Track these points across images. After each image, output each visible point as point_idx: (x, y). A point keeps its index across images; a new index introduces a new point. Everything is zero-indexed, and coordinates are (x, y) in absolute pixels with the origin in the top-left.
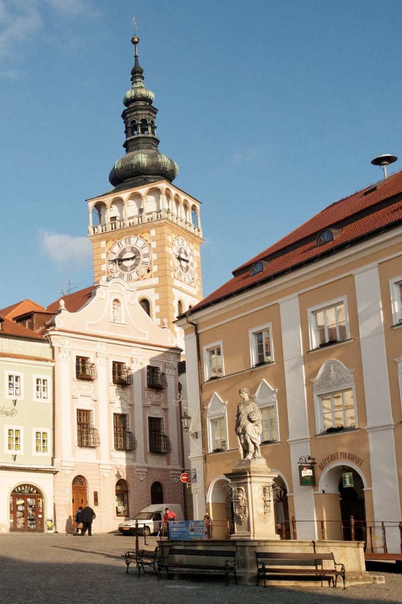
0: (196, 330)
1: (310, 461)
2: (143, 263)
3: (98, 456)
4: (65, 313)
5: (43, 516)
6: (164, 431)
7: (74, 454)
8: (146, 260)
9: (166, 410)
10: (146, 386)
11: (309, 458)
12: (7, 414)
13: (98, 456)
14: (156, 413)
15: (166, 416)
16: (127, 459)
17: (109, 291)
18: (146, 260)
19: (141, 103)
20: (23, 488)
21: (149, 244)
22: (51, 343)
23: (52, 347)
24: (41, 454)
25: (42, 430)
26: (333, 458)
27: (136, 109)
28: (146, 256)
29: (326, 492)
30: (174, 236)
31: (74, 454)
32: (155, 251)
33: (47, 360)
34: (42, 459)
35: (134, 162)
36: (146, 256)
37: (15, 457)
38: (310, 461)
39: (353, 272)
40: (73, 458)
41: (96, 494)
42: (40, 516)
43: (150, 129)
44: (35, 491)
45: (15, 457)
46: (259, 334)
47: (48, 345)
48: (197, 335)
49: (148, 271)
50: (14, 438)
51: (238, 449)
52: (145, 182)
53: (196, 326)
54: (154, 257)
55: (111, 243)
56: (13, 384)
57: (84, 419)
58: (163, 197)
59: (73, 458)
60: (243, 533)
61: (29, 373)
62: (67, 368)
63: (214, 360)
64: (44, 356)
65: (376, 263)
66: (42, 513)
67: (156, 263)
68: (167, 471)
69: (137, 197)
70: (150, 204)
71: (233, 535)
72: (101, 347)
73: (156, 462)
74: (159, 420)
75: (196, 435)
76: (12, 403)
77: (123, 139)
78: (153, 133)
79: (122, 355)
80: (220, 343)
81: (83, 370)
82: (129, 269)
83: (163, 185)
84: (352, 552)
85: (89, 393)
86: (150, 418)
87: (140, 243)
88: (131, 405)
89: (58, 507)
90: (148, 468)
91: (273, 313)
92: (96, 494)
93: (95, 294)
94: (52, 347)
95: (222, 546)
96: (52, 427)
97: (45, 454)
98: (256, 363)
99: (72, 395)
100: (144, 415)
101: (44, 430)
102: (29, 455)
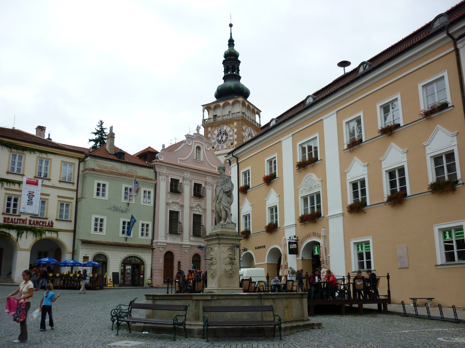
0: (238, 160)
1: (295, 239)
2: (230, 140)
5: (144, 277)
8: (231, 138)
10: (193, 195)
11: (295, 237)
12: (122, 212)
14: (175, 208)
17: (194, 141)
18: (231, 138)
20: (131, 259)
21: (233, 130)
22: (155, 169)
23: (156, 172)
24: (144, 237)
25: (146, 223)
26: (308, 236)
28: (231, 136)
29: (304, 258)
30: (246, 126)
31: (166, 238)
32: (236, 133)
33: (151, 180)
34: (146, 240)
36: (231, 136)
37: (126, 239)
38: (295, 239)
39: (322, 118)
41: (179, 263)
42: (142, 276)
43: (236, 71)
44: (139, 261)
45: (126, 239)
46: (270, 162)
47: (152, 170)
48: (238, 164)
49: (232, 144)
54: (235, 136)
55: (213, 128)
56: (127, 193)
57: (174, 217)
60: (213, 287)
62: (164, 186)
64: (150, 177)
65: (335, 111)
66: (143, 275)
67: (236, 140)
71: (206, 289)
72: (187, 175)
74: (200, 216)
76: (126, 206)
77: (223, 74)
78: (238, 73)
81: (175, 187)
82: (217, 138)
83: (241, 99)
84: (297, 302)
86: (194, 215)
87: (228, 129)
88: (204, 210)
90: (167, 243)
92: (179, 263)
94: (156, 172)
95: (168, 299)
96: (153, 221)
97: (146, 238)
98: (301, 213)
100: (166, 209)
101: (148, 223)
102: (137, 237)
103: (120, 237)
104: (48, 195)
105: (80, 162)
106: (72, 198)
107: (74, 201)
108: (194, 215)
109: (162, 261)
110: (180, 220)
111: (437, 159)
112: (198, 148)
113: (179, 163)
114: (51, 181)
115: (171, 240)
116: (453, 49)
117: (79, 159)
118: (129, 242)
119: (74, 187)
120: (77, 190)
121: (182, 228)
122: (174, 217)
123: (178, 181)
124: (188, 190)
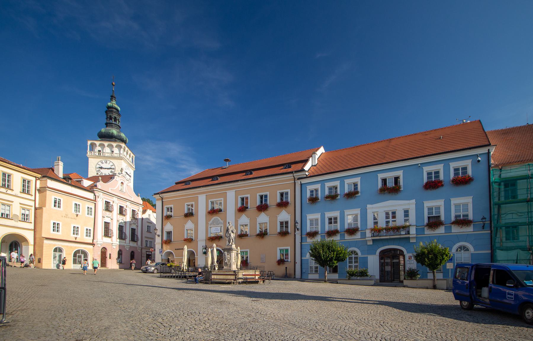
3: (112, 240)
4: (101, 182)
6: (136, 233)
7: (102, 239)
9: (137, 226)
13: (112, 240)
14: (108, 220)
15: (112, 222)
16: (119, 242)
19: (114, 110)
27: (112, 111)
31: (102, 239)
34: (89, 240)
35: (111, 132)
37: (76, 238)
40: (101, 240)
41: (110, 254)
45: (76, 238)
48: (162, 202)
50: (76, 230)
51: (153, 239)
52: (115, 141)
53: (162, 198)
57: (107, 225)
58: (122, 150)
59: (101, 240)
61: (84, 205)
62: (101, 205)
63: (500, 255)
68: (136, 248)
69: (111, 146)
70: (116, 150)
72: (115, 199)
73: (133, 244)
74: (134, 229)
75: (159, 236)
77: (105, 121)
79: (123, 204)
80: (172, 206)
81: (108, 207)
83: (123, 145)
85: (110, 216)
86: (105, 222)
89: (93, 256)
91: (196, 200)
92: (110, 254)
93: (114, 178)
99: (102, 216)
100: (103, 220)
102: (82, 237)
103: (72, 237)
104: (12, 202)
105: (36, 180)
106: (32, 206)
107: (33, 209)
108: (105, 222)
109: (100, 253)
110: (111, 228)
111: (282, 223)
112: (122, 183)
113: (110, 191)
114: (277, 264)
115: (107, 240)
116: (471, 217)
117: (36, 177)
118: (77, 240)
119: (33, 198)
120: (35, 201)
121: (112, 232)
122: (107, 225)
123: (122, 207)
124: (116, 210)
